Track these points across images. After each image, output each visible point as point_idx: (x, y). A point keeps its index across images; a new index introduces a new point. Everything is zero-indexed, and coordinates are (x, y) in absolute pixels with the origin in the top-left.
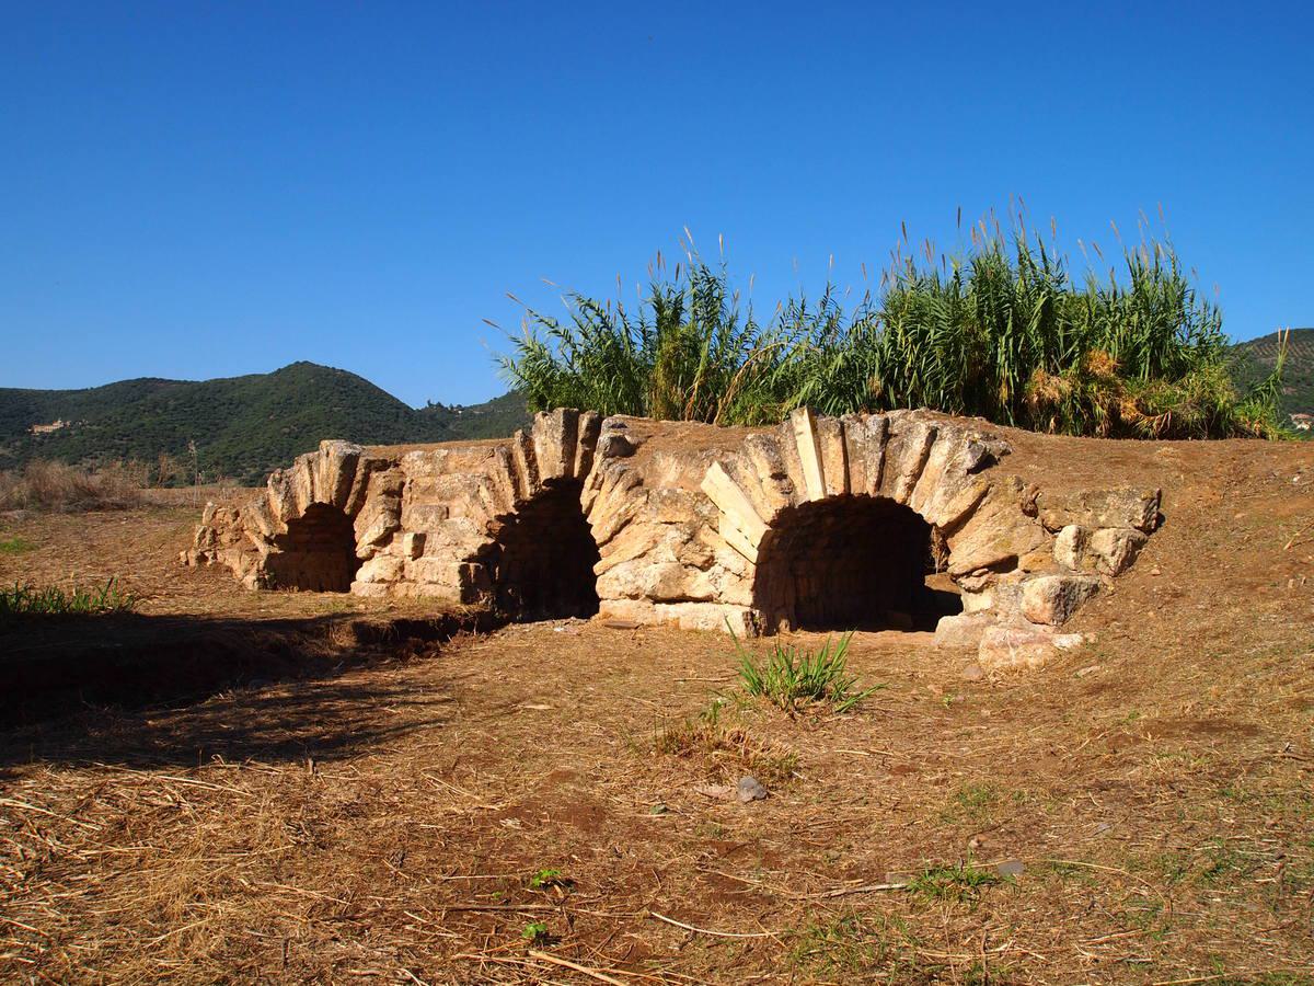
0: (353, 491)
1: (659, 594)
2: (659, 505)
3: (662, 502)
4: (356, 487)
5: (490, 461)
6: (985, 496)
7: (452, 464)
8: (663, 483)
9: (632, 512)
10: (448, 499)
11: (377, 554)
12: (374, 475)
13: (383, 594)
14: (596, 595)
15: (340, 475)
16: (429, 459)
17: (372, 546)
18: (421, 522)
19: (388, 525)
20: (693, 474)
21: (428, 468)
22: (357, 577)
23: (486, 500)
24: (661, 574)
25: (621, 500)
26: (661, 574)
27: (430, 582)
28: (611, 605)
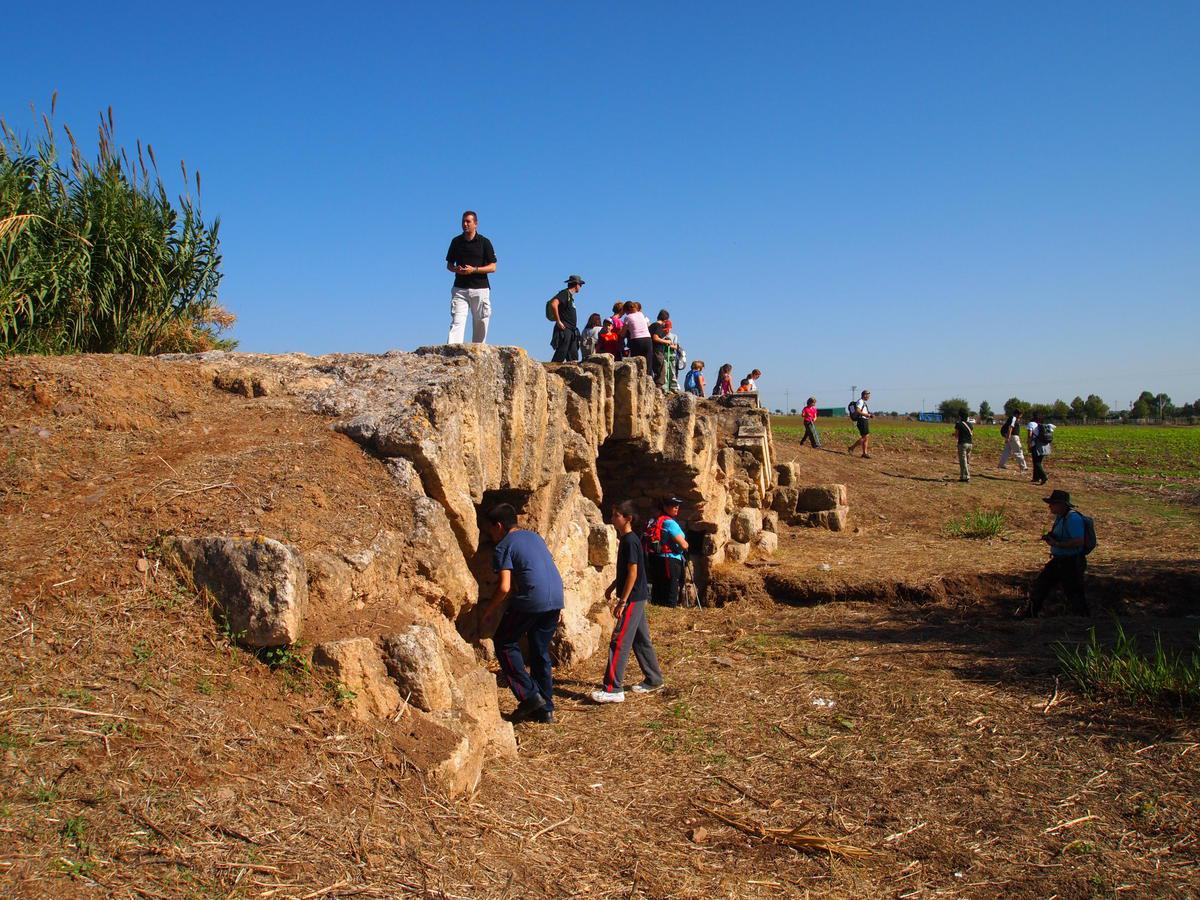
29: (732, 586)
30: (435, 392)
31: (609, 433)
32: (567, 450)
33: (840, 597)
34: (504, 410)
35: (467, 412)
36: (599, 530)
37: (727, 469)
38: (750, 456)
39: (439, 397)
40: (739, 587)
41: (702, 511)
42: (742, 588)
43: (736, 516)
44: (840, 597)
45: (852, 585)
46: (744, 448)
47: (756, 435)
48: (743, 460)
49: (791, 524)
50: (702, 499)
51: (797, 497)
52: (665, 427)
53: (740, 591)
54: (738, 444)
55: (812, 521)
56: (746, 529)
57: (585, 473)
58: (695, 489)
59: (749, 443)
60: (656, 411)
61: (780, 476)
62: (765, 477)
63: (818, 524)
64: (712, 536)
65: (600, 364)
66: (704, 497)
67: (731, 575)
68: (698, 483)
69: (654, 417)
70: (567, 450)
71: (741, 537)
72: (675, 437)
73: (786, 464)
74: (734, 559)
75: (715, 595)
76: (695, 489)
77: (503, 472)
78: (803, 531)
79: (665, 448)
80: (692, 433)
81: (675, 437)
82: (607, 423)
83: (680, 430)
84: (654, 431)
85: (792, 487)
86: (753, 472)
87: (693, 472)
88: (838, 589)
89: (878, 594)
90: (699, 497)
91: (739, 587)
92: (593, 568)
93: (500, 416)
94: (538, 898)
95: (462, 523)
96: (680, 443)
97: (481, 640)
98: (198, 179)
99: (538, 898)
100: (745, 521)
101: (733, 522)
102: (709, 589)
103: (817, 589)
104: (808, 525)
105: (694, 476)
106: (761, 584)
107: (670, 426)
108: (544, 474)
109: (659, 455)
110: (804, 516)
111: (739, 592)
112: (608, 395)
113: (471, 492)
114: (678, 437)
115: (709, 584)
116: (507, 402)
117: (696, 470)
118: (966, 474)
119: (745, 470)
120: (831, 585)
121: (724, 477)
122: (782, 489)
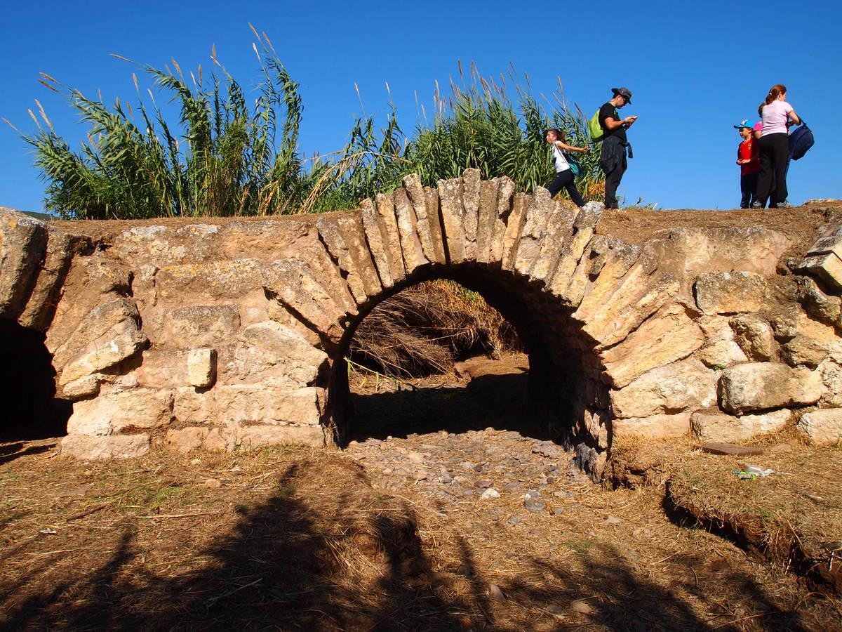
0: (39, 287)
1: (762, 404)
2: (718, 293)
3: (723, 288)
4: (46, 280)
5: (302, 241)
6: (810, 253)
7: (231, 245)
8: (687, 265)
9: (661, 302)
10: (231, 297)
11: (104, 388)
12: (81, 261)
13: (144, 450)
14: (66, 431)
15: (24, 260)
16: (180, 239)
17: (100, 376)
18: (195, 331)
19: (137, 340)
20: (733, 254)
21: (180, 251)
22: (68, 430)
23: (318, 296)
24: (764, 379)
25: (641, 287)
26: (764, 379)
27: (249, 423)
28: (638, 425)
40: (636, 472)
66: (597, 338)
86: (813, 310)
111: (632, 478)
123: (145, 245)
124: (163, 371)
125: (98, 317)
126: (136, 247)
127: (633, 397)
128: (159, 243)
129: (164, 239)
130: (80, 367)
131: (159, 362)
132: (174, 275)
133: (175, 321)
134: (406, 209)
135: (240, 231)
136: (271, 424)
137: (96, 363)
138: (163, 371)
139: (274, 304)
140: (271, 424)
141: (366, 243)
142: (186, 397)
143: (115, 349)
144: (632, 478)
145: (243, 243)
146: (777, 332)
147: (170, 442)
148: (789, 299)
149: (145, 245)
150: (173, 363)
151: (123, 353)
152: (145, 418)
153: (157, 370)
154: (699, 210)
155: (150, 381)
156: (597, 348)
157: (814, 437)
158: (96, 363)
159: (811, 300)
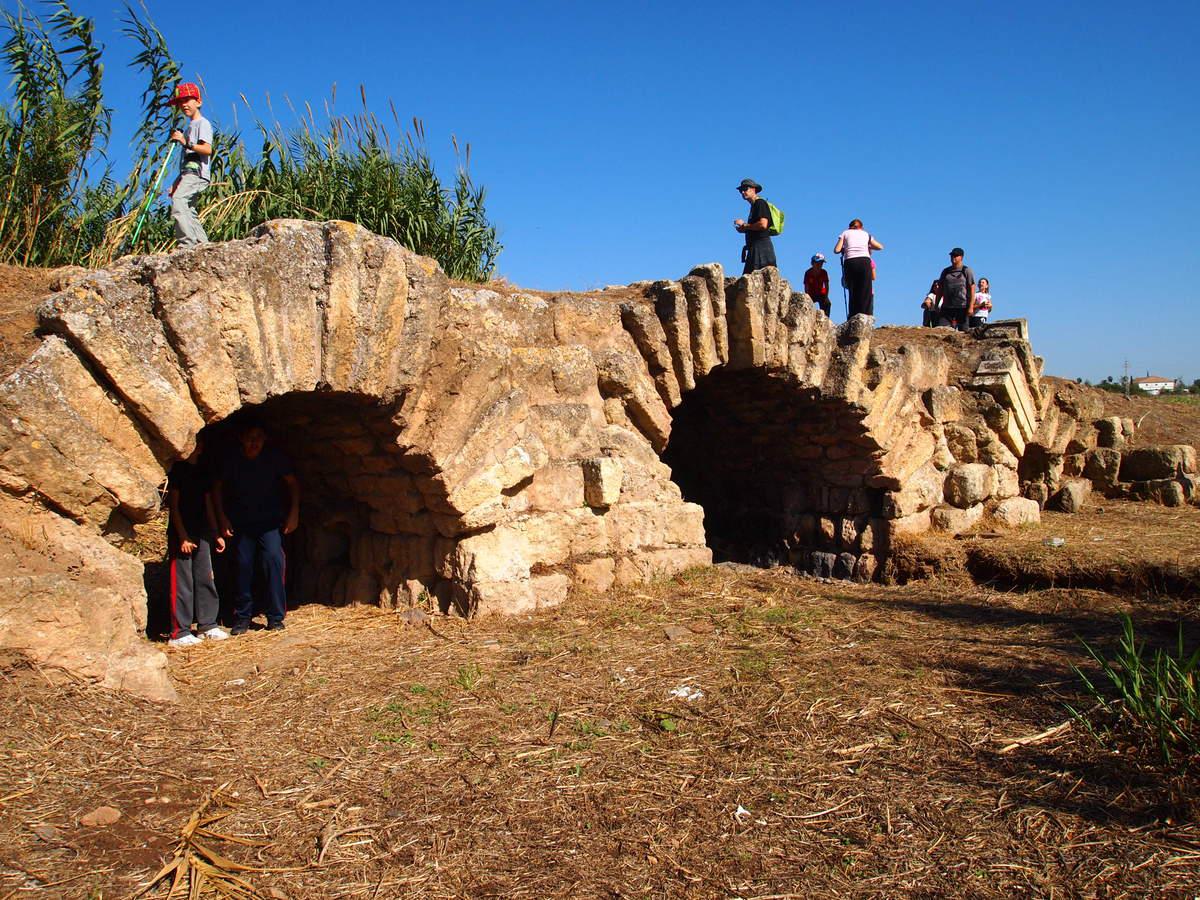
29: (918, 560)
30: (159, 267)
31: (721, 358)
32: (601, 372)
33: (1061, 581)
34: (323, 297)
35: (225, 293)
36: (593, 463)
37: (935, 411)
38: (990, 398)
39: (163, 272)
40: (929, 562)
41: (880, 463)
42: (933, 562)
43: (952, 473)
44: (1061, 581)
45: (1081, 567)
46: (982, 388)
47: (999, 371)
48: (979, 404)
49: (1109, 497)
50: (878, 448)
51: (1118, 461)
52: (828, 357)
53: (931, 568)
54: (975, 384)
55: (1139, 493)
56: (964, 490)
57: (628, 401)
58: (867, 434)
59: (989, 382)
60: (814, 336)
61: (1099, 434)
62: (1020, 427)
63: (1145, 496)
64: (893, 494)
65: (702, 276)
66: (881, 444)
67: (921, 545)
68: (871, 427)
69: (812, 345)
70: (601, 372)
71: (957, 499)
72: (838, 369)
73: (1108, 419)
74: (941, 527)
75: (896, 570)
76: (867, 434)
77: (322, 371)
78: (1121, 506)
79: (825, 382)
80: (862, 362)
81: (838, 369)
82: (718, 349)
83: (844, 359)
84: (810, 362)
85: (1117, 450)
86: (992, 420)
87: (859, 411)
88: (1060, 571)
89: (1117, 580)
90: (872, 445)
91: (929, 562)
92: (589, 510)
93: (318, 304)
94: (713, 894)
95: (147, 414)
96: (843, 375)
97: (408, 581)
98: (468, 149)
99: (713, 894)
100: (962, 480)
101: (948, 484)
102: (890, 561)
103: (1029, 569)
104: (1132, 498)
105: (863, 417)
106: (961, 561)
107: (834, 355)
108: (402, 377)
109: (816, 390)
110: (1126, 486)
111: (928, 568)
112: (716, 313)
113: (240, 389)
114: (842, 368)
115: (890, 556)
116: (326, 287)
117: (863, 409)
118: (13, 203)
119: (981, 416)
120: (1050, 564)
121: (932, 423)
122: (1100, 451)
123: (477, 315)
124: (554, 488)
125: (504, 414)
126: (468, 318)
127: (65, 574)
128: (493, 314)
129: (499, 309)
130: (484, 485)
131: (548, 477)
132: (524, 361)
133: (545, 423)
134: (707, 301)
135: (572, 308)
136: (663, 548)
137: (504, 479)
138: (554, 488)
139: (617, 405)
140: (663, 548)
141: (260, 324)
142: (586, 522)
143: (526, 458)
144: (928, 568)
145: (574, 324)
146: (979, 438)
147: (584, 581)
148: (972, 411)
149: (477, 315)
150: (562, 479)
151: (536, 464)
152: (552, 554)
153: (548, 489)
154: (895, 326)
155: (542, 502)
156: (877, 453)
157: (1010, 521)
158: (504, 479)
159: (995, 412)
